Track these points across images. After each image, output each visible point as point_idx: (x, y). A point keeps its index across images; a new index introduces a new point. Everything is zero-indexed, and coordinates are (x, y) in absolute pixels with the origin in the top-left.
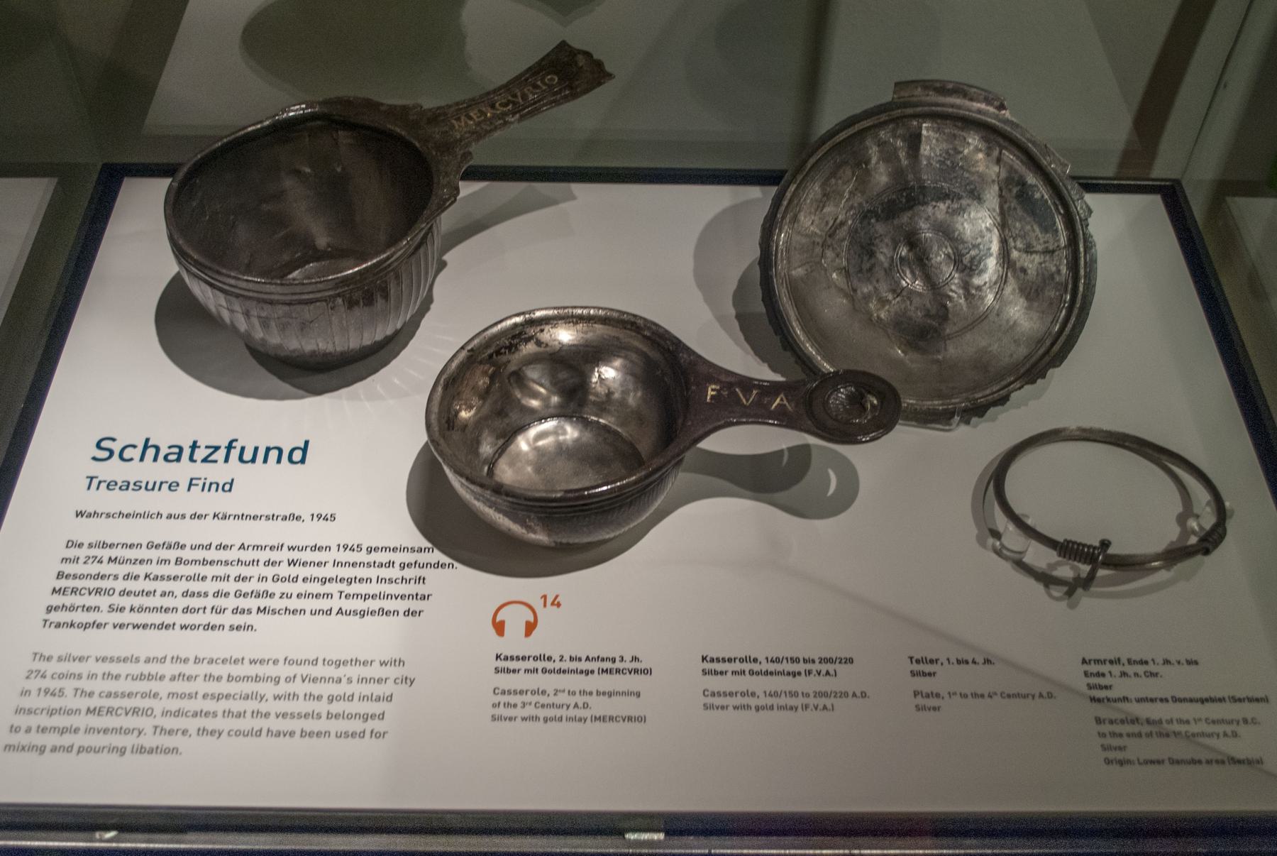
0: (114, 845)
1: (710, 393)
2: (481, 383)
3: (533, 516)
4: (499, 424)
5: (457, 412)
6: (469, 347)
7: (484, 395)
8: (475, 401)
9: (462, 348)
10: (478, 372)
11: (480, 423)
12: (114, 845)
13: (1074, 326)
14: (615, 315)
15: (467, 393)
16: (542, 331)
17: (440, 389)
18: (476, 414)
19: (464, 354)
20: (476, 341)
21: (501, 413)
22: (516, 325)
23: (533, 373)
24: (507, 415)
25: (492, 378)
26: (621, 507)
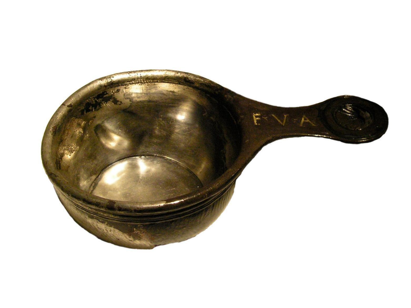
0: (234, 180)
1: (255, 120)
2: (77, 132)
3: (139, 224)
4: (91, 165)
5: (62, 155)
6: (69, 104)
7: (81, 141)
8: (74, 146)
9: (63, 104)
10: (75, 124)
11: (78, 161)
12: (234, 180)
13: (187, 214)
14: (172, 74)
15: (67, 139)
16: (118, 91)
17: (50, 135)
18: (76, 156)
19: (65, 109)
20: (73, 100)
21: (91, 156)
22: (101, 86)
23: (109, 125)
24: (95, 158)
25: (84, 129)
26: (206, 210)
